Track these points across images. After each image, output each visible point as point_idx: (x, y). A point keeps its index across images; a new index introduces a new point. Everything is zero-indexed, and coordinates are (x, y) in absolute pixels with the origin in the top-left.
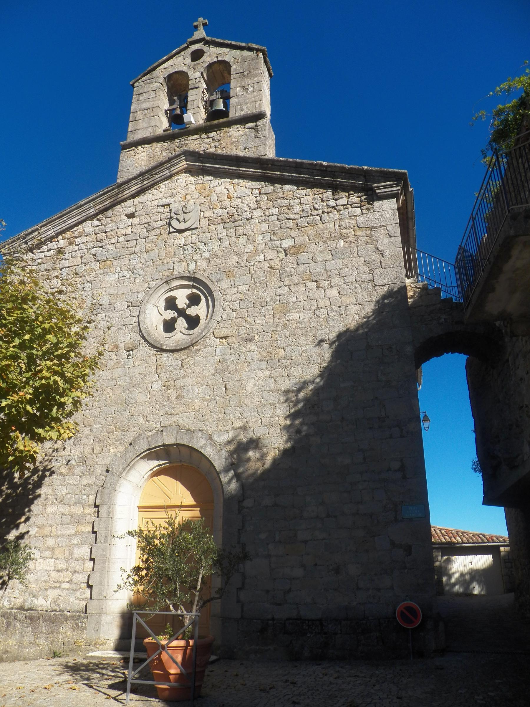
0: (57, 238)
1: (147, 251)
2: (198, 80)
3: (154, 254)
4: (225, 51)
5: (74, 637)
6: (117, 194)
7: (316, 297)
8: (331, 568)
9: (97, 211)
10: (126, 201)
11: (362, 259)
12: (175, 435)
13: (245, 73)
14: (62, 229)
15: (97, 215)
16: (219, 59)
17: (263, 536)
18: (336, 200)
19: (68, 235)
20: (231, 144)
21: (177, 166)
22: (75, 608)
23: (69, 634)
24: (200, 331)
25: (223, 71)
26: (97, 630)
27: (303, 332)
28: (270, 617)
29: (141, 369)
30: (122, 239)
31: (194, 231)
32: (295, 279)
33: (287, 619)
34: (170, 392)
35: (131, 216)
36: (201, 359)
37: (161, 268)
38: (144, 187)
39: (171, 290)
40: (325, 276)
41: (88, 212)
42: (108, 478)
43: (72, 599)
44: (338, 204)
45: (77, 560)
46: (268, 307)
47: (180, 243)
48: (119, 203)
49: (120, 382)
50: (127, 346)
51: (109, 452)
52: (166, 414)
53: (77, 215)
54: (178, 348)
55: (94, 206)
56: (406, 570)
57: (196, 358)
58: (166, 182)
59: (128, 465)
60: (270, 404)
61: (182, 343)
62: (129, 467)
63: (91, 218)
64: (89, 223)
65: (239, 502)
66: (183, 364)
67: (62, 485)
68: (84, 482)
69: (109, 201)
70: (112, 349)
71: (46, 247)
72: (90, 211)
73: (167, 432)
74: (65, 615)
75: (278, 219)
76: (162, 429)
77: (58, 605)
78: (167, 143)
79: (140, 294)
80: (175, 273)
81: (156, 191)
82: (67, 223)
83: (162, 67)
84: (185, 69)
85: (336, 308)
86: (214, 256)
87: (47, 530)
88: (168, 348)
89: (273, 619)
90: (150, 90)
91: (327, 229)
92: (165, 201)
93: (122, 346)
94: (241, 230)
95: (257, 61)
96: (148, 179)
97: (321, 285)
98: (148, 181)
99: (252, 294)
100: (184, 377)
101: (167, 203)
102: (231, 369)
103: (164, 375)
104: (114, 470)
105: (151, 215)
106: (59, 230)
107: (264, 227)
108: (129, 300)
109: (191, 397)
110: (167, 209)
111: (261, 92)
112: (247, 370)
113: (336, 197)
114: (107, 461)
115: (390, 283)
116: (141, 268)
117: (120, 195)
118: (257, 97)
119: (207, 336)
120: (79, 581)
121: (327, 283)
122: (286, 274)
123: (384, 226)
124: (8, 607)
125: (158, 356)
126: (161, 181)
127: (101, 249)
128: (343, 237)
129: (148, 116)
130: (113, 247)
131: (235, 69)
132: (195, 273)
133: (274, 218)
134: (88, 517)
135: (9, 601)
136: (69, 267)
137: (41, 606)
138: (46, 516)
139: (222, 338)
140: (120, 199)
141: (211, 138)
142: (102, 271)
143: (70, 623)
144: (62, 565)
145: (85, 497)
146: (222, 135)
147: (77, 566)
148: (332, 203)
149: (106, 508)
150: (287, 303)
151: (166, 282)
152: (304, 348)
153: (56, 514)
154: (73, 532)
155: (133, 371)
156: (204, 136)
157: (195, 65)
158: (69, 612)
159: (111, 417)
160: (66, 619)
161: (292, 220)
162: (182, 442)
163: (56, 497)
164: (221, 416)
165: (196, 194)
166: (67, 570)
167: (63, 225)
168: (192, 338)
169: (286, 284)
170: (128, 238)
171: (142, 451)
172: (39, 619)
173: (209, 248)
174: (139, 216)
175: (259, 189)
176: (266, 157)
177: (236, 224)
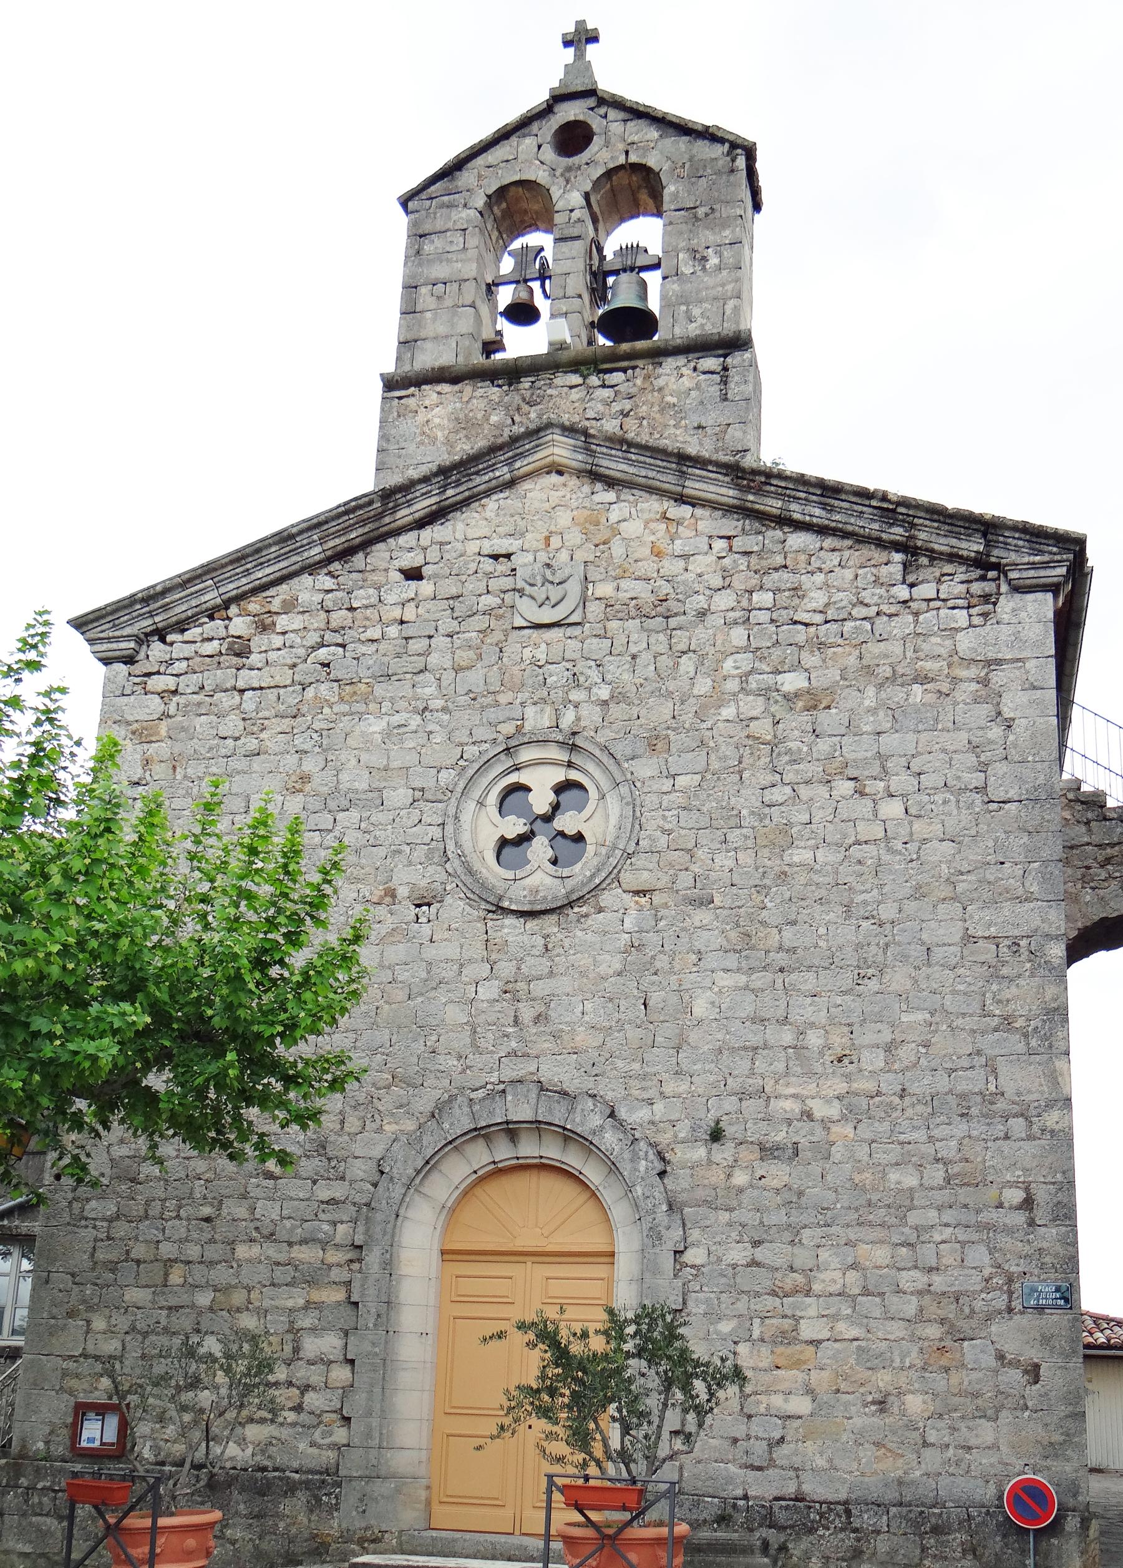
0: (227, 608)
1: (458, 669)
2: (576, 215)
3: (474, 678)
4: (648, 137)
5: (313, 1525)
6: (380, 516)
7: (853, 816)
8: (870, 1399)
9: (329, 553)
10: (399, 534)
11: (964, 736)
12: (533, 1101)
13: (701, 212)
14: (240, 591)
15: (329, 560)
16: (633, 158)
18: (912, 585)
19: (253, 606)
20: (662, 411)
21: (530, 459)
22: (312, 1464)
23: (302, 1518)
24: (588, 874)
25: (639, 187)
26: (364, 1511)
27: (823, 892)
28: (739, 1492)
29: (451, 950)
30: (393, 631)
31: (570, 631)
32: (813, 769)
33: (777, 1499)
34: (520, 1005)
35: (413, 574)
36: (590, 937)
37: (492, 714)
38: (447, 502)
39: (517, 768)
40: (876, 770)
41: (306, 554)
42: (380, 1188)
43: (302, 1446)
44: (914, 597)
45: (310, 1363)
46: (744, 831)
47: (538, 656)
48: (382, 538)
49: (403, 975)
50: (416, 895)
51: (380, 1130)
52: (512, 1054)
53: (278, 559)
54: (538, 908)
55: (322, 540)
56: (1027, 1414)
57: (579, 933)
58: (502, 495)
59: (427, 1162)
60: (745, 1048)
61: (545, 898)
62: (429, 1166)
63: (311, 568)
64: (306, 579)
65: (676, 1252)
66: (550, 946)
67: (269, 1199)
68: (325, 1195)
69: (360, 531)
70: (382, 898)
71: (199, 630)
72: (312, 553)
73: (515, 1095)
74: (289, 1478)
75: (772, 621)
76: (502, 1087)
77: (269, 1457)
78: (499, 386)
79: (444, 774)
80: (528, 727)
81: (476, 515)
82: (253, 577)
83: (480, 161)
84: (541, 175)
85: (900, 846)
86: (619, 696)
87: (238, 1298)
88: (514, 907)
89: (746, 1497)
90: (450, 225)
91: (886, 656)
92: (502, 545)
93: (403, 892)
94: (681, 640)
95: (732, 178)
96: (458, 483)
97: (867, 790)
98: (458, 490)
99: (709, 795)
100: (551, 974)
101: (504, 552)
102: (658, 964)
103: (506, 969)
104: (395, 1170)
105: (463, 578)
106: (235, 592)
107: (738, 636)
108: (418, 784)
109: (568, 1019)
110: (503, 567)
111: (739, 273)
112: (695, 969)
113: (911, 578)
114: (377, 1152)
115: (1023, 797)
116: (445, 710)
117: (387, 520)
118: (729, 287)
119: (604, 885)
120: (318, 1407)
121: (882, 784)
122: (787, 758)
123: (1019, 660)
124: (152, 1459)
125: (490, 924)
126: (488, 493)
127: (341, 650)
128: (922, 679)
129: (448, 302)
130: (370, 649)
131: (675, 195)
132: (574, 734)
133: (764, 616)
134: (335, 1271)
135: (156, 1449)
136: (261, 688)
137: (232, 1459)
138: (235, 1266)
139: (637, 893)
140: (386, 528)
141: (612, 387)
142: (345, 708)
143: (302, 1496)
145: (326, 1227)
146: (639, 382)
147: (315, 1375)
148: (903, 592)
149: (378, 1254)
150: (789, 824)
151: (508, 749)
152: (822, 931)
153: (260, 1262)
154: (301, 1302)
155: (430, 952)
156: (594, 380)
157: (569, 169)
158: (297, 1472)
159: (383, 1054)
160: (291, 1488)
161: (806, 625)
162: (549, 1119)
163: (259, 1224)
164: (636, 1066)
165: (574, 537)
166: (290, 1384)
167: (244, 581)
168: (569, 888)
169: (786, 780)
170: (409, 631)
171: (459, 1132)
172: (230, 1486)
173: (609, 677)
174: (436, 576)
175: (729, 538)
177: (673, 623)
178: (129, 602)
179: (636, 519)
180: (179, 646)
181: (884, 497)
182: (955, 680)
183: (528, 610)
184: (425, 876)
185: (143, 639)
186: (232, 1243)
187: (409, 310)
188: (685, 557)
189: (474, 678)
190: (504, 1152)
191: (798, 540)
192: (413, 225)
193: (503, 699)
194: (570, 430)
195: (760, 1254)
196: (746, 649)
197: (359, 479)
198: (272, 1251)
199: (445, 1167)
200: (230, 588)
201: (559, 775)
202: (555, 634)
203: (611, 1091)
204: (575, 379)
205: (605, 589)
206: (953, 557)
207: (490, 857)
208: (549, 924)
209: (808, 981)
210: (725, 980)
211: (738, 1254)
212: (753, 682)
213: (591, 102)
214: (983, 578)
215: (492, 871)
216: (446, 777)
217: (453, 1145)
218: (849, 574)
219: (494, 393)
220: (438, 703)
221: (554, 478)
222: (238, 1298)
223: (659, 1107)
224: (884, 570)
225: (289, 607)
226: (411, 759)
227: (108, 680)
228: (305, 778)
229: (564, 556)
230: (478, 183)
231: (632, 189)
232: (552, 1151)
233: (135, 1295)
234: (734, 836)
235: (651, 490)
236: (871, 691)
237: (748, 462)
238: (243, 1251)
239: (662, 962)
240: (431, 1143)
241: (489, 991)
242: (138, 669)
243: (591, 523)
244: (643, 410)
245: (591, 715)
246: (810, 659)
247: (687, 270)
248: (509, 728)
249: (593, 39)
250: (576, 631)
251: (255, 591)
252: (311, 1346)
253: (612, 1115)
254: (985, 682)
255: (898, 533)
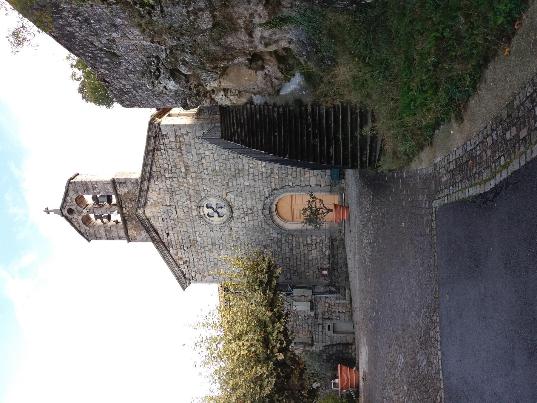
15: (167, 249)
16: (74, 201)
17: (302, 179)
19: (177, 261)
29: (240, 224)
35: (168, 234)
40: (199, 155)
48: (161, 240)
52: (257, 214)
53: (168, 258)
63: (169, 252)
64: (171, 252)
87: (302, 253)
92: (161, 220)
93: (230, 233)
94: (177, 189)
103: (242, 215)
114: (276, 234)
116: (195, 228)
126: (150, 223)
128: (180, 147)
144: (314, 247)
147: (314, 241)
155: (240, 227)
156: (124, 206)
165: (158, 208)
176: (11, 7)
177: (173, 190)
178: (179, 282)
179: (153, 196)
180: (186, 272)
181: (145, 156)
182: (180, 142)
183: (174, 215)
184: (226, 229)
185: (185, 278)
186: (293, 255)
187: (113, 238)
188: (160, 189)
189: (188, 223)
190: (275, 213)
191: (154, 169)
192: (94, 239)
193: (192, 218)
194: (136, 211)
195: (290, 173)
196: (177, 178)
197: (150, 245)
198: (294, 249)
199: (274, 219)
200: (174, 265)
201: (205, 208)
202: (178, 210)
203: (263, 198)
204: (124, 209)
205: (168, 202)
206: (155, 142)
207: (222, 218)
208: (234, 209)
209: (241, 167)
210: (242, 180)
211: (290, 177)
212: (184, 176)
213: (63, 209)
214: (158, 137)
215: (224, 219)
216: (207, 227)
217: (274, 221)
218: (160, 160)
219: (129, 223)
220: (193, 229)
221: (146, 212)
222: (302, 253)
223: (265, 190)
224: (159, 154)
225: (177, 255)
226: (205, 233)
227: (194, 283)
228: (210, 250)
229: (162, 210)
230: (83, 228)
231: (80, 200)
232: (274, 206)
233: (303, 269)
234: (215, 179)
235: (147, 195)
236: (184, 156)
237: (140, 180)
238: (294, 253)
239: (239, 190)
240: (274, 226)
241: (247, 218)
242: (191, 278)
243: (154, 205)
244: (130, 197)
245: (193, 204)
246: (178, 167)
247: (98, 190)
248: (197, 217)
249: (47, 209)
250: (177, 207)
251: (174, 261)
252: (309, 242)
253: (267, 198)
254: (180, 136)
255: (151, 153)
